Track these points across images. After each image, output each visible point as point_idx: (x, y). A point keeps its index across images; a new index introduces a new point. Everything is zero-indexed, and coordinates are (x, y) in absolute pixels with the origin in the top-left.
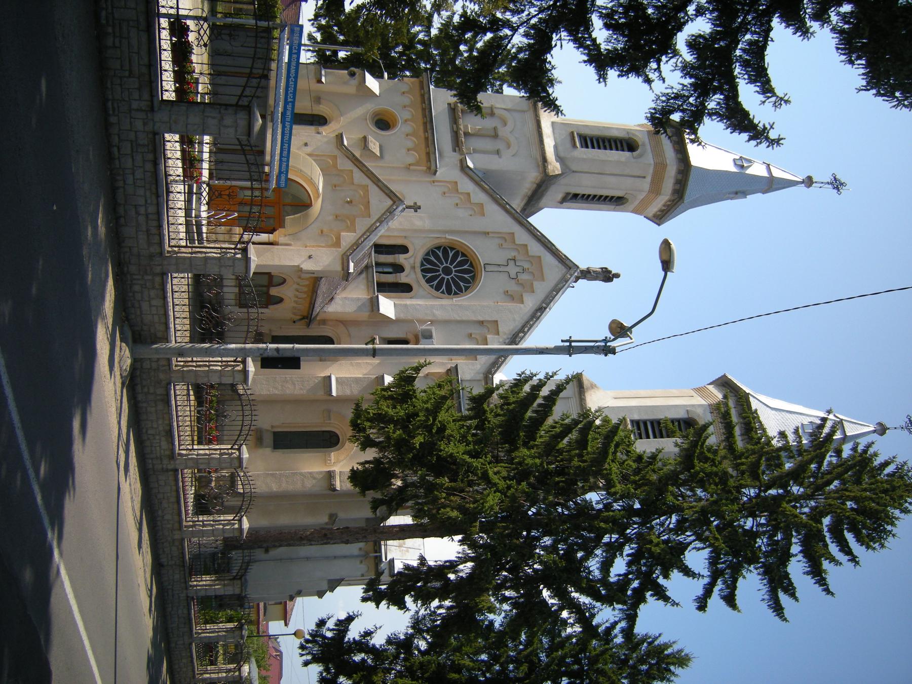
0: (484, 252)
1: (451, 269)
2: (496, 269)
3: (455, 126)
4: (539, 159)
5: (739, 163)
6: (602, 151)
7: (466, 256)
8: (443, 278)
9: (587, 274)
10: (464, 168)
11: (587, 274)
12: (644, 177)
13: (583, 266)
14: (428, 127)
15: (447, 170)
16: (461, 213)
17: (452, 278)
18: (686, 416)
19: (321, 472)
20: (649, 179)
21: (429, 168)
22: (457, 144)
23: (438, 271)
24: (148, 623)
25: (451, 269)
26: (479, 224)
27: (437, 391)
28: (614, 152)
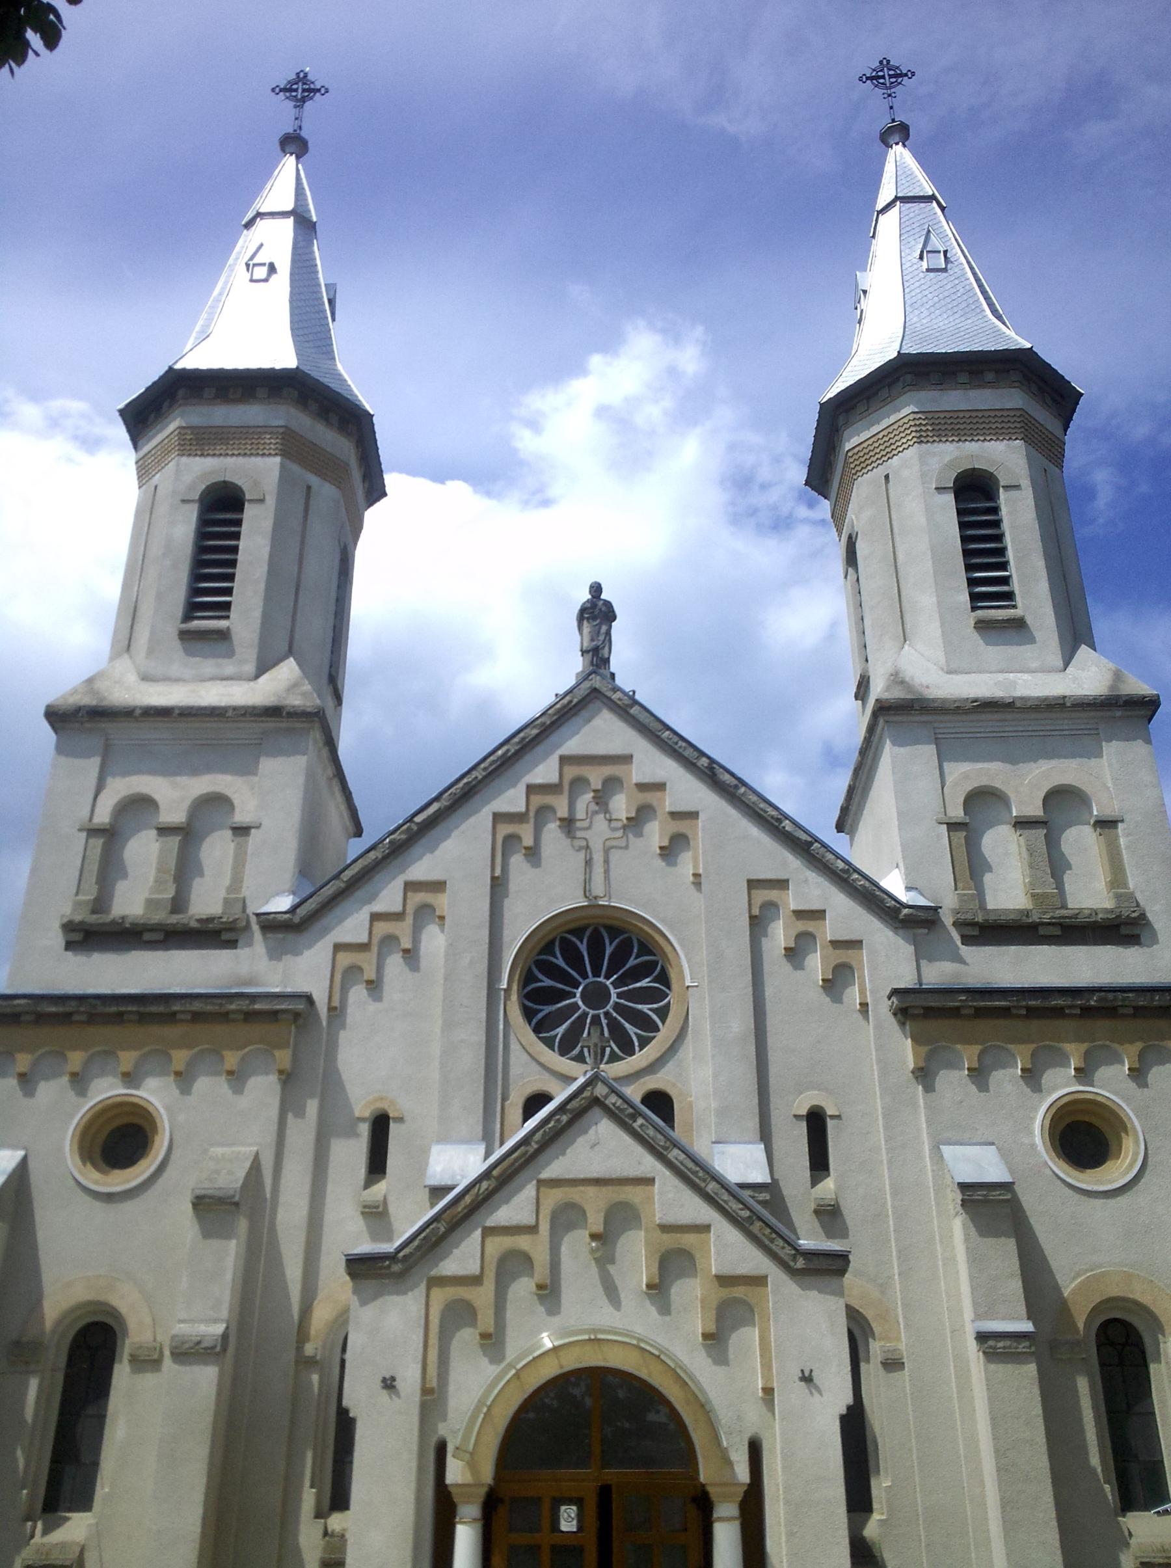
0: (546, 894)
1: (589, 976)
2: (598, 869)
3: (147, 936)
4: (271, 724)
5: (261, 273)
6: (240, 572)
7: (551, 943)
8: (619, 996)
9: (597, 656)
10: (286, 930)
11: (597, 656)
12: (309, 488)
13: (576, 664)
14: (154, 1009)
15: (306, 971)
16: (434, 941)
17: (597, 974)
18: (950, 498)
19: (974, 1259)
20: (314, 480)
21: (297, 1015)
22: (216, 935)
23: (575, 1007)
24: (563, 1249)
25: (589, 976)
26: (466, 903)
27: (81, 897)
28: (242, 544)
